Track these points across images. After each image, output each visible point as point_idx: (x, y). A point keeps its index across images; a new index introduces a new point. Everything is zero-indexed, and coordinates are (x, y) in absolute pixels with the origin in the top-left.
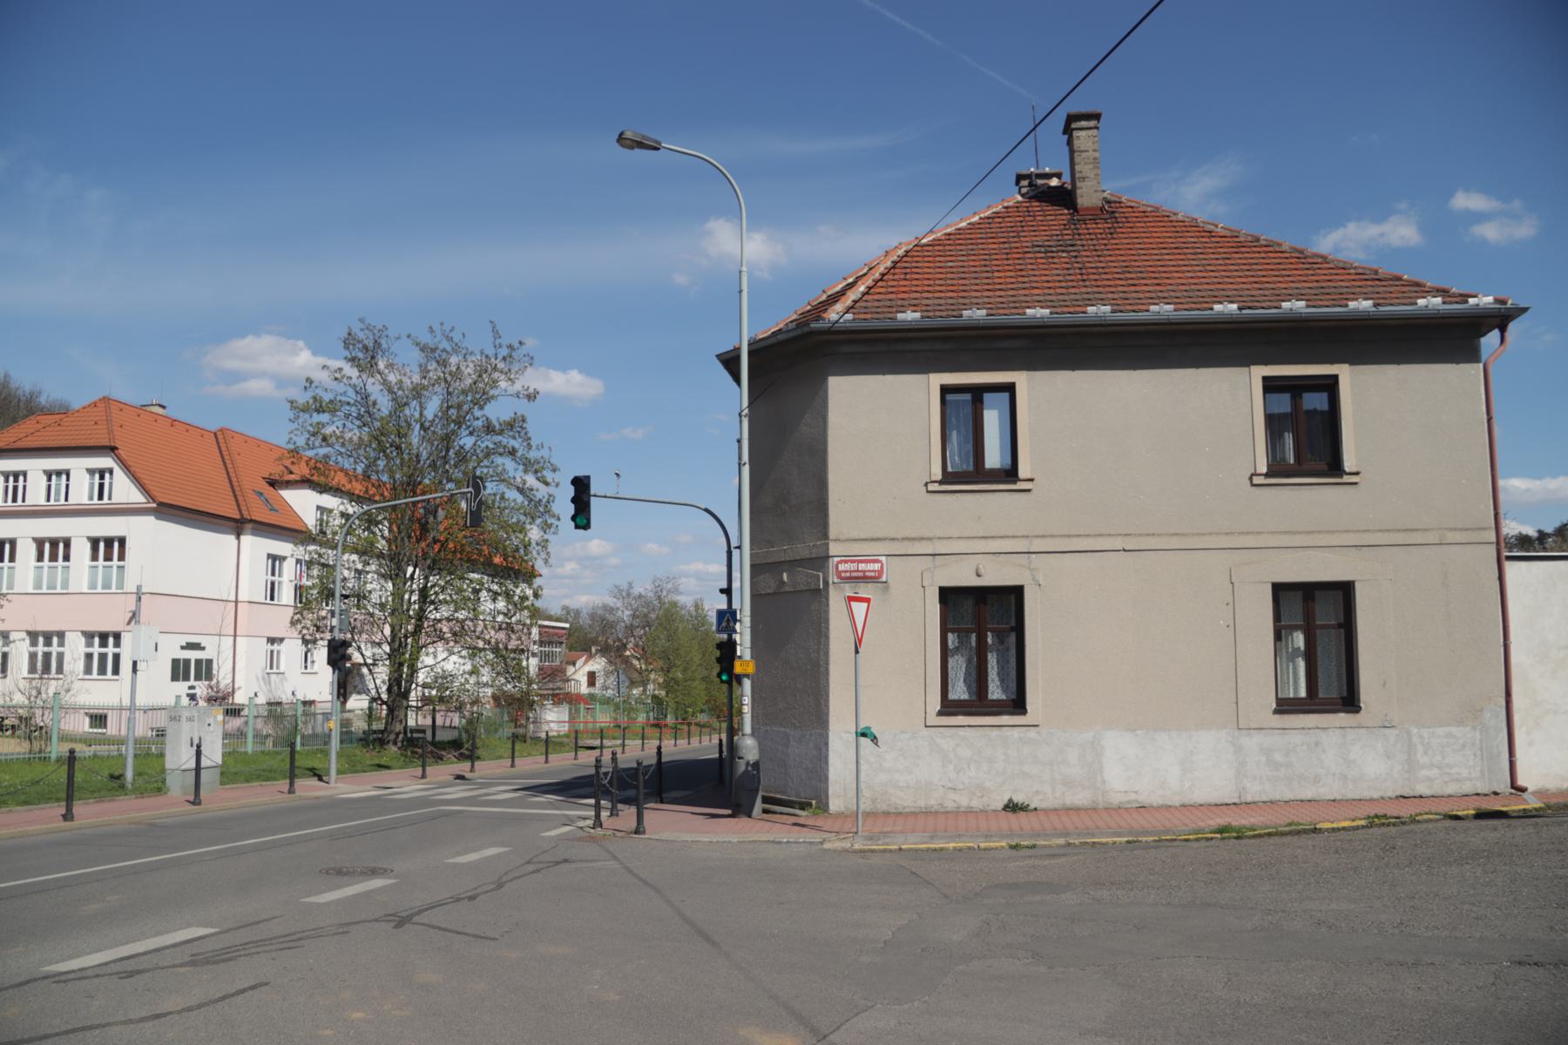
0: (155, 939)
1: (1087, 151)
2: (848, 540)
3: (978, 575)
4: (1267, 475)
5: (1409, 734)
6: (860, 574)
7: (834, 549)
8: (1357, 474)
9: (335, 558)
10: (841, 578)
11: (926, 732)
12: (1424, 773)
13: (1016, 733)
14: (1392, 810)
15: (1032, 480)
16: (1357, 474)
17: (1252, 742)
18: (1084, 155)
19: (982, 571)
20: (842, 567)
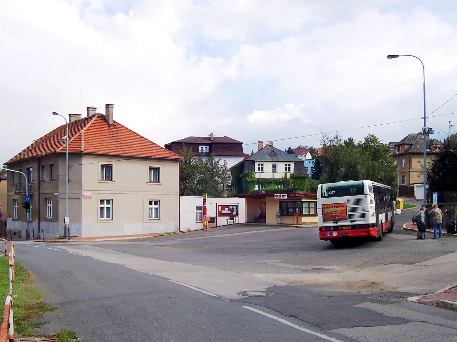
0: (201, 291)
1: (111, 112)
2: (85, 190)
3: (106, 197)
4: (234, 220)
5: (167, 223)
6: (87, 196)
7: (83, 192)
8: (161, 183)
9: (380, 297)
10: (84, 197)
11: (97, 223)
12: (168, 229)
13: (111, 223)
14: (364, 292)
15: (114, 181)
16: (161, 183)
17: (146, 224)
18: (111, 113)
19: (107, 196)
20: (84, 195)
